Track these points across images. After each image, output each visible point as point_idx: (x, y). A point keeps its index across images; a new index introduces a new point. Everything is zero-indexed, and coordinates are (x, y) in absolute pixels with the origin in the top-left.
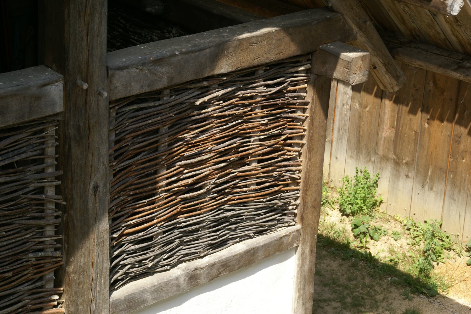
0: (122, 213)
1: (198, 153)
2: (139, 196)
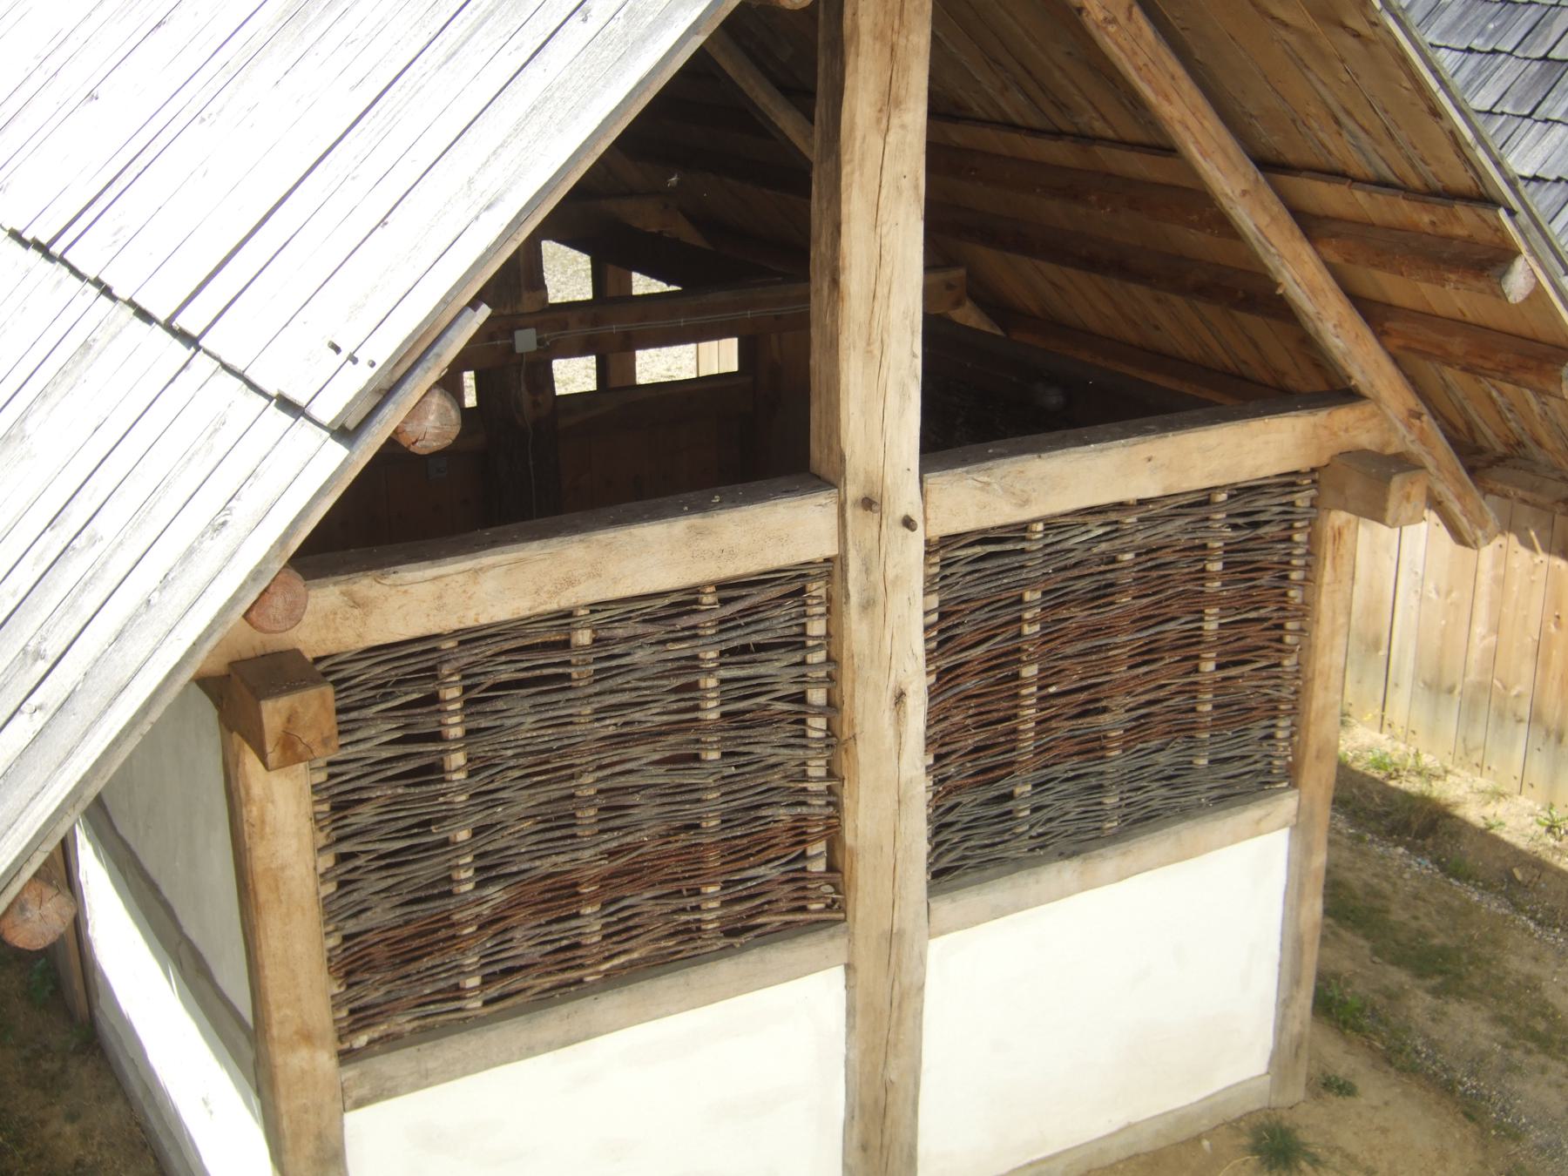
0: (953, 747)
1: (1461, 141)
2: (984, 717)
